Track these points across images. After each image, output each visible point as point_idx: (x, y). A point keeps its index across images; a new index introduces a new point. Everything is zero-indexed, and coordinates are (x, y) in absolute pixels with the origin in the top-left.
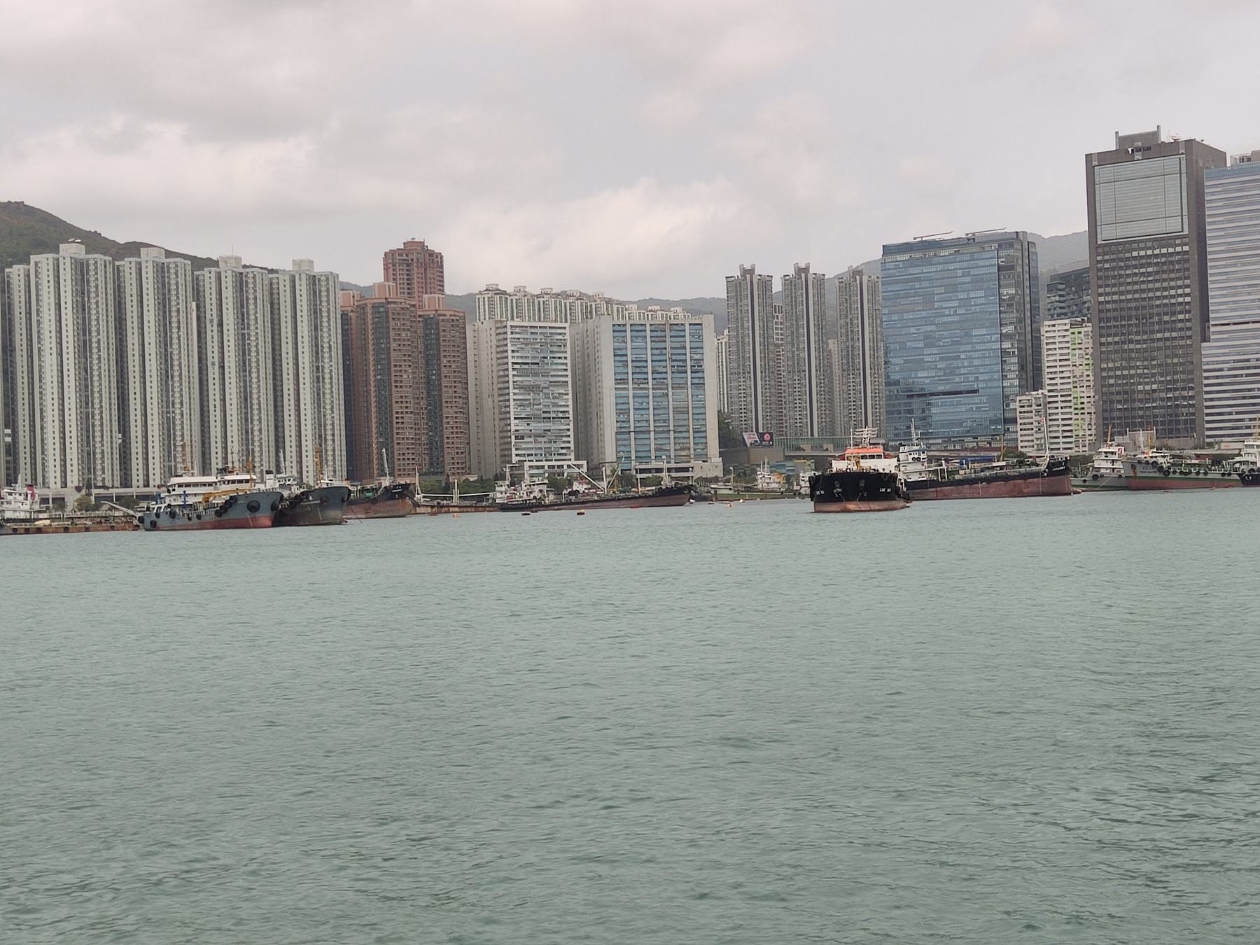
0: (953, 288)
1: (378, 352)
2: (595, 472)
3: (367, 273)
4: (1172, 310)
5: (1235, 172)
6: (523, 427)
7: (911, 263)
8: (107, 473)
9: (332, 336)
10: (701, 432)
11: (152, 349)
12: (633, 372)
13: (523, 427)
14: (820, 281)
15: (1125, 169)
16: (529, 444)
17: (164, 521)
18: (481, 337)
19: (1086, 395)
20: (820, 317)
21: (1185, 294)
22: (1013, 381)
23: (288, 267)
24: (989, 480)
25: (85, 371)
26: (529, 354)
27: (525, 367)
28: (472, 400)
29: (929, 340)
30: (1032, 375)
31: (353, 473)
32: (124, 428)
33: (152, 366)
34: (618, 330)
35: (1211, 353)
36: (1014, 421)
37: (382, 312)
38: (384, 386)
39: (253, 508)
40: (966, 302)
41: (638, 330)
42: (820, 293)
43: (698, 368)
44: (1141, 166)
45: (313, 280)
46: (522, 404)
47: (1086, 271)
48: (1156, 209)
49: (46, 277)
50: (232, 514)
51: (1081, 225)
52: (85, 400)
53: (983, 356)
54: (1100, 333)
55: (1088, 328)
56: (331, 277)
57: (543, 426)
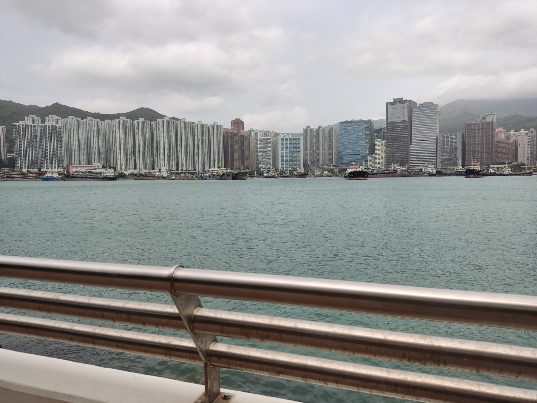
0: (355, 132)
1: (231, 143)
2: (276, 170)
3: (227, 125)
4: (404, 138)
5: (419, 107)
6: (261, 160)
7: (346, 126)
8: (174, 168)
9: (221, 139)
10: (299, 162)
11: (183, 141)
12: (285, 149)
13: (261, 160)
14: (312, 129)
15: (395, 106)
16: (262, 164)
17: (208, 178)
18: (253, 139)
19: (383, 156)
20: (324, 137)
21: (407, 134)
22: (367, 152)
23: (212, 124)
24: (381, 174)
25: (169, 145)
26: (263, 144)
27: (262, 147)
28: (64, 152)
29: (349, 143)
30: (372, 151)
31: (463, 166)
32: (177, 158)
33: (183, 144)
34: (282, 139)
35: (411, 146)
36: (367, 161)
37: (232, 134)
38: (232, 150)
39: (228, 176)
40: (357, 135)
41: (286, 139)
42: (324, 133)
43: (299, 148)
44: (398, 105)
45: (218, 126)
46: (261, 155)
47: (383, 129)
48: (401, 115)
49: (161, 124)
50: (224, 177)
51: (384, 118)
52: (169, 152)
53: (361, 148)
54: (387, 143)
55: (385, 141)
56: (221, 126)
57: (265, 160)
